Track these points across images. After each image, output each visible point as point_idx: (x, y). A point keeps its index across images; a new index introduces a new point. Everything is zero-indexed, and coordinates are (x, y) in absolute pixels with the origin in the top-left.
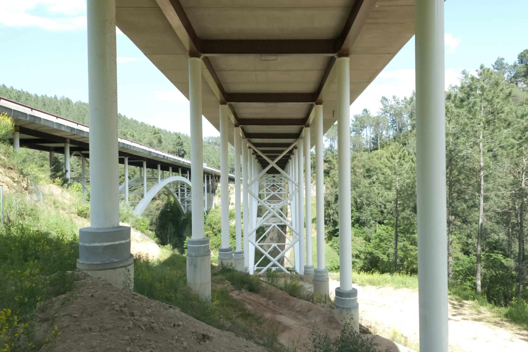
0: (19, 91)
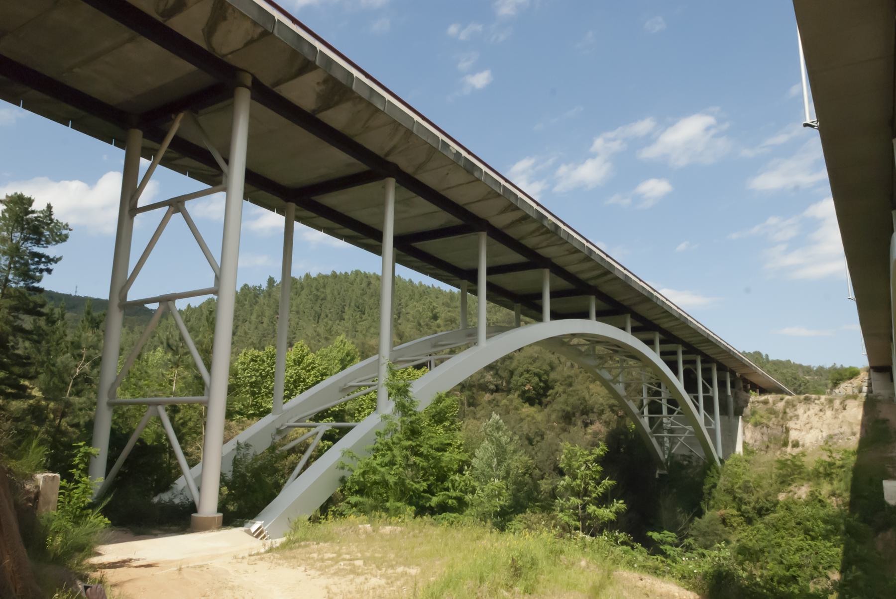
0: (429, 287)
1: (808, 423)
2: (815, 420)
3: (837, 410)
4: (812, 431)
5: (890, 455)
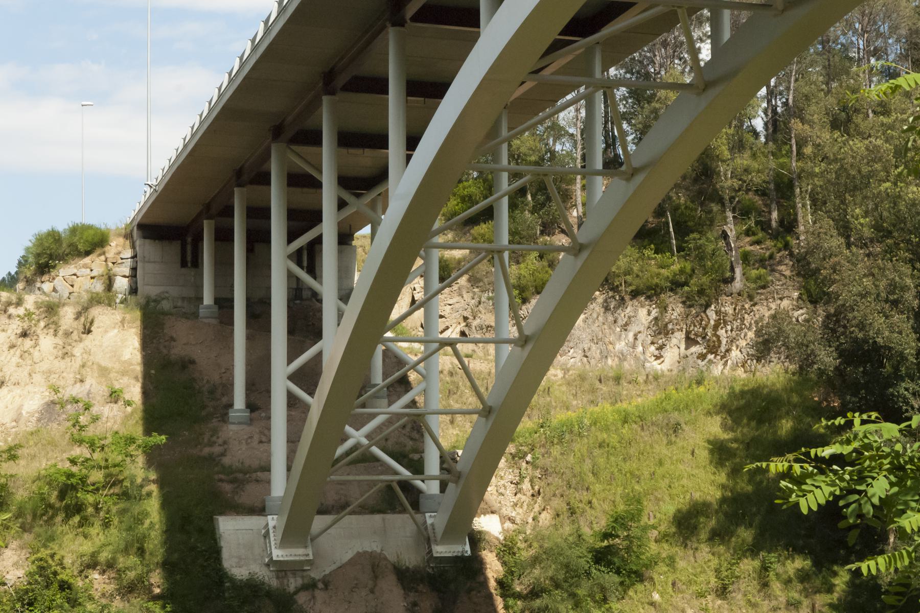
3: (68, 334)
5: (206, 451)
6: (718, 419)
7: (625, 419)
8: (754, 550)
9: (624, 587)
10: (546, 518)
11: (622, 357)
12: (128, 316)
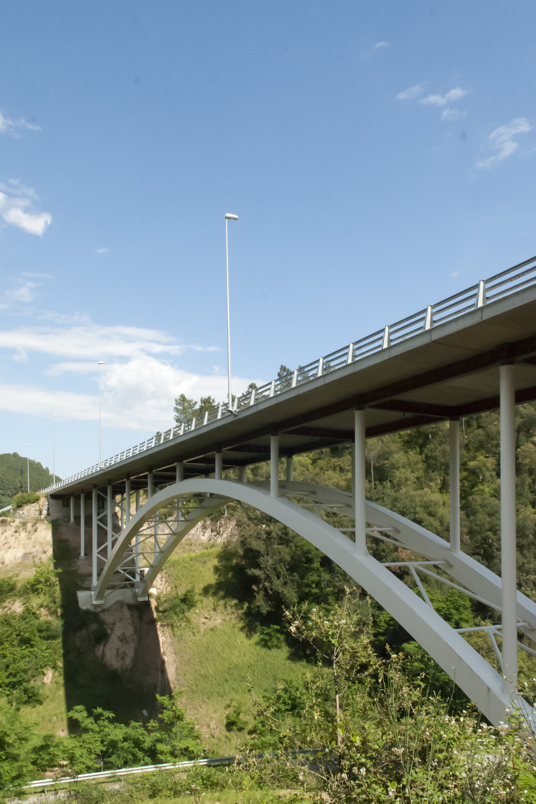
1: (6, 543)
2: (12, 540)
3: (29, 532)
4: (10, 550)
5: (73, 569)
6: (217, 560)
7: (191, 559)
8: (223, 598)
9: (189, 609)
10: (169, 588)
11: (193, 535)
12: (48, 526)
